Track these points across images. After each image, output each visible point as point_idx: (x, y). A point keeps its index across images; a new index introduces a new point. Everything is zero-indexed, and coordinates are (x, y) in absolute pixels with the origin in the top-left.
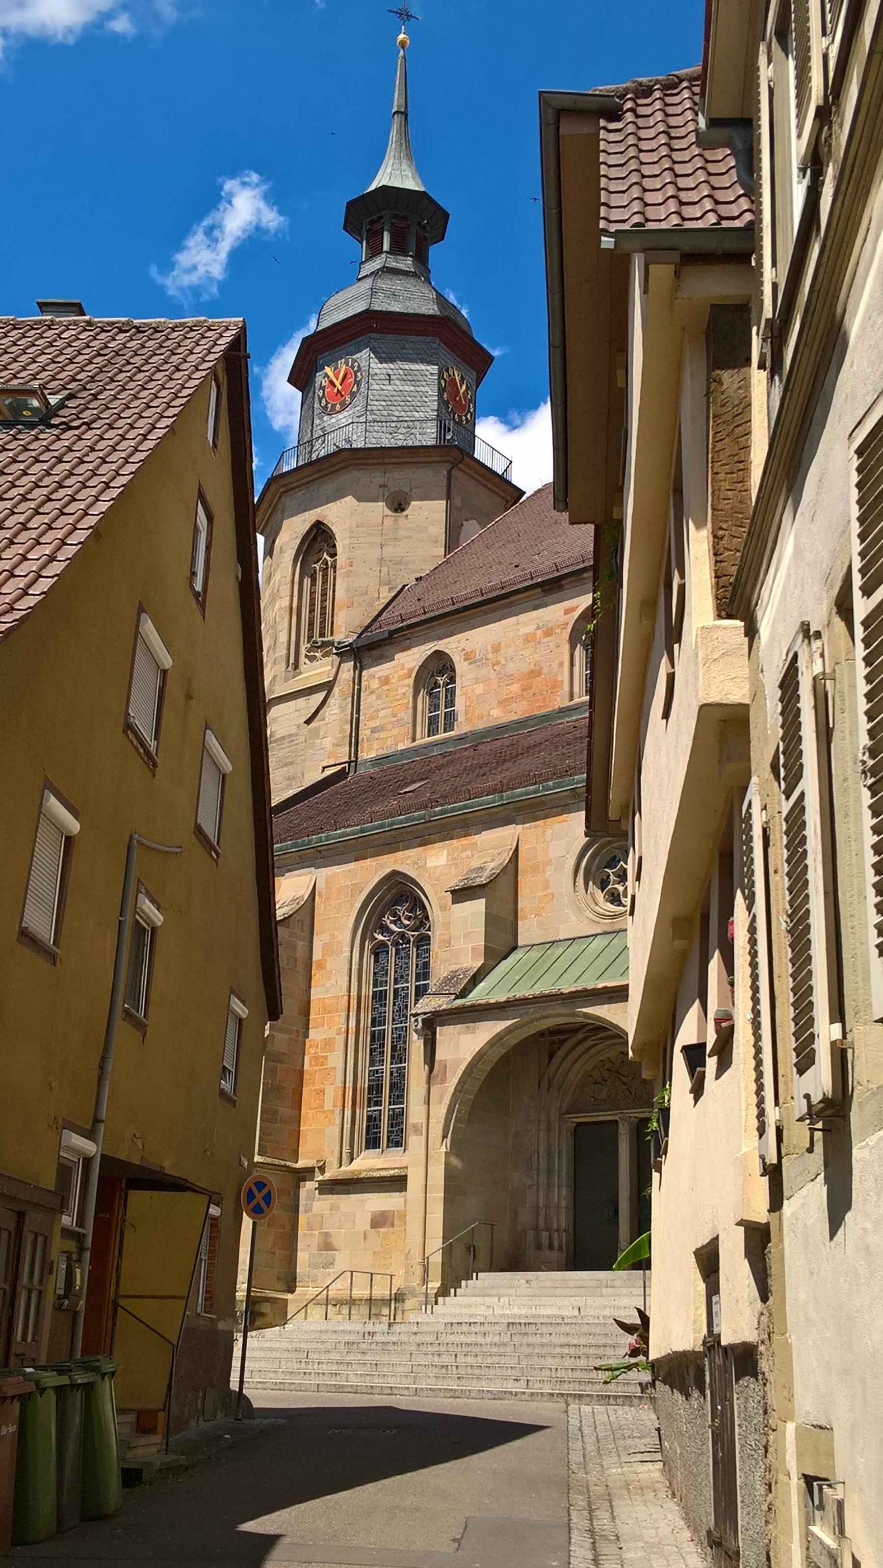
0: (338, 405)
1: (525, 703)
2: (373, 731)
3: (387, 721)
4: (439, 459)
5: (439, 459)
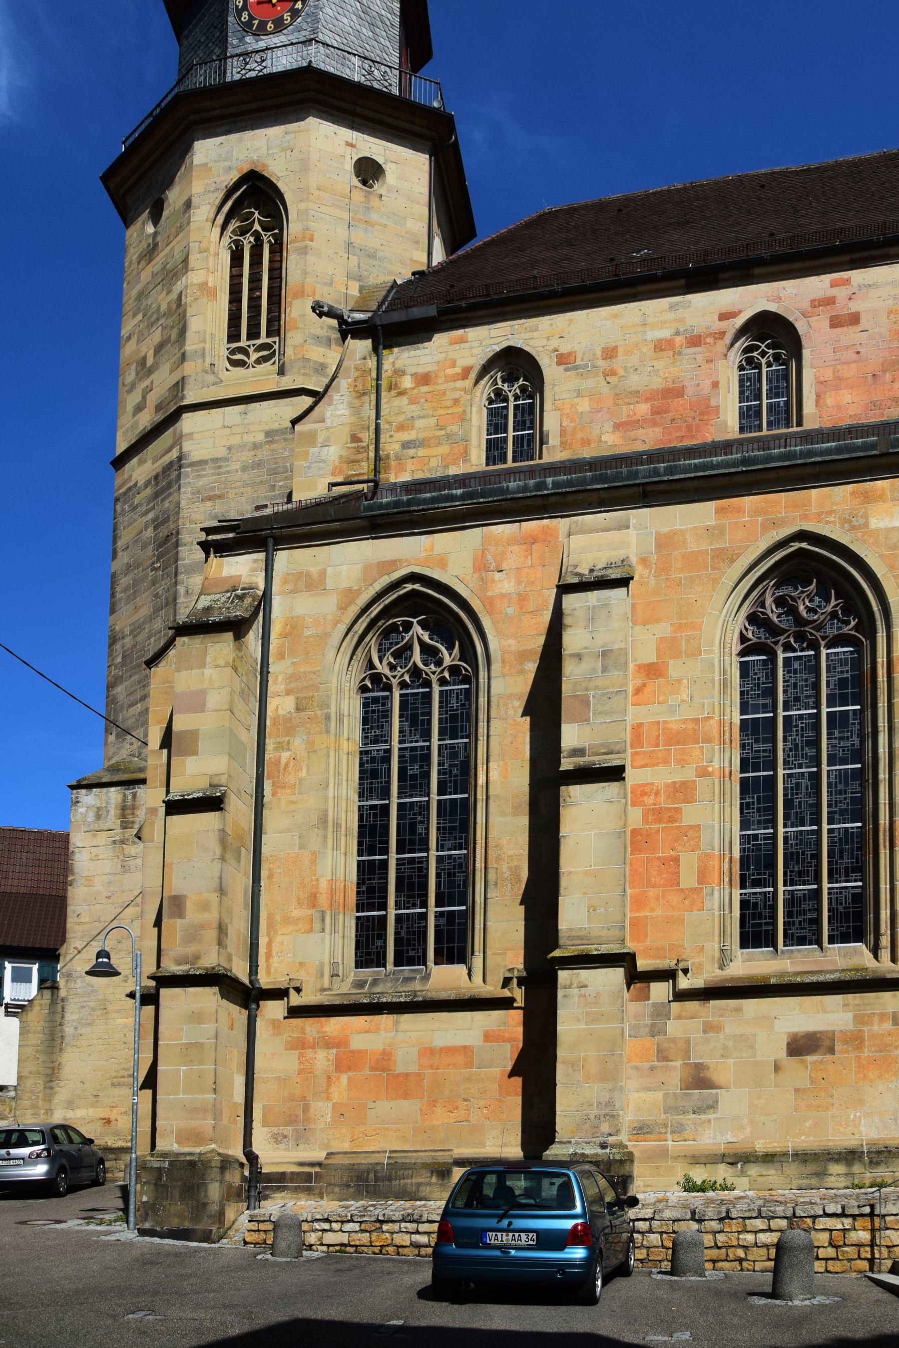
0: (270, 24)
1: (658, 431)
2: (406, 445)
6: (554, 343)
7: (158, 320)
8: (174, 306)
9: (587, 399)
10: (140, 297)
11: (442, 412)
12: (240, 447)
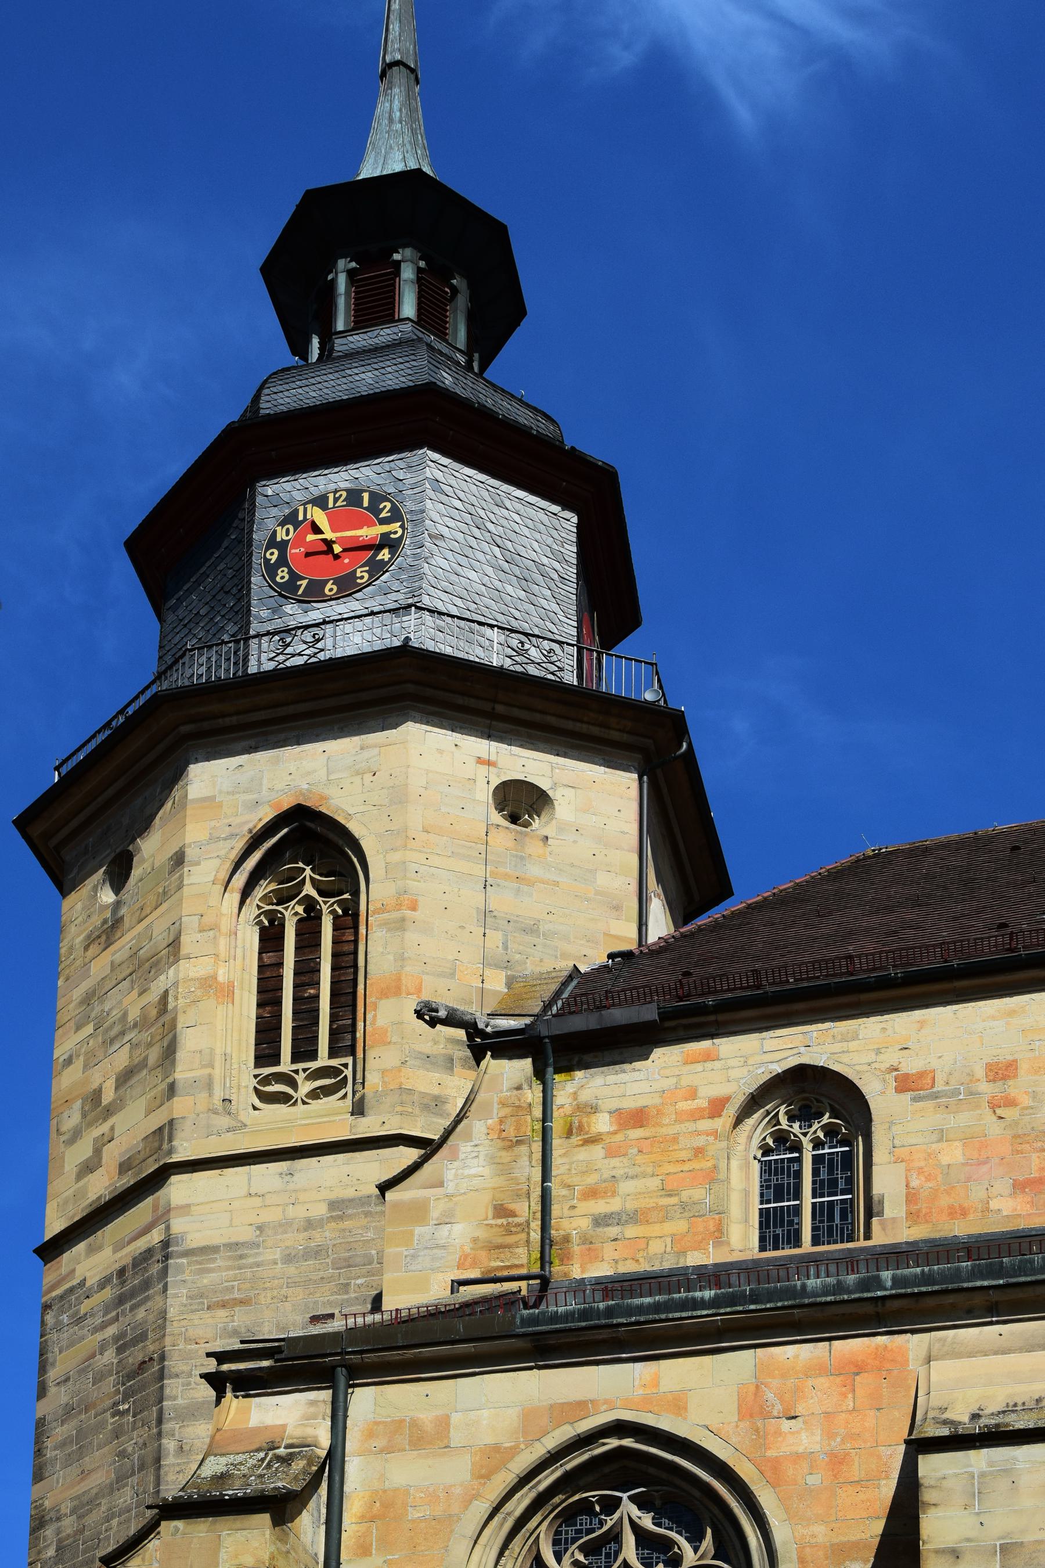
3: (650, 1203)
4: (625, 738)
5: (625, 738)
6: (891, 1057)
7: (123, 1033)
8: (154, 1013)
9: (957, 1143)
10: (88, 1000)
11: (672, 1168)
12: (281, 1225)
